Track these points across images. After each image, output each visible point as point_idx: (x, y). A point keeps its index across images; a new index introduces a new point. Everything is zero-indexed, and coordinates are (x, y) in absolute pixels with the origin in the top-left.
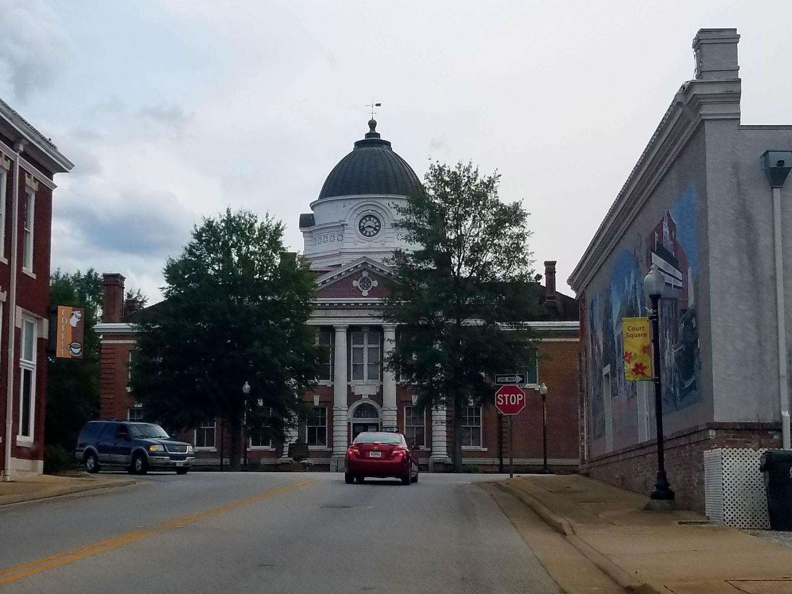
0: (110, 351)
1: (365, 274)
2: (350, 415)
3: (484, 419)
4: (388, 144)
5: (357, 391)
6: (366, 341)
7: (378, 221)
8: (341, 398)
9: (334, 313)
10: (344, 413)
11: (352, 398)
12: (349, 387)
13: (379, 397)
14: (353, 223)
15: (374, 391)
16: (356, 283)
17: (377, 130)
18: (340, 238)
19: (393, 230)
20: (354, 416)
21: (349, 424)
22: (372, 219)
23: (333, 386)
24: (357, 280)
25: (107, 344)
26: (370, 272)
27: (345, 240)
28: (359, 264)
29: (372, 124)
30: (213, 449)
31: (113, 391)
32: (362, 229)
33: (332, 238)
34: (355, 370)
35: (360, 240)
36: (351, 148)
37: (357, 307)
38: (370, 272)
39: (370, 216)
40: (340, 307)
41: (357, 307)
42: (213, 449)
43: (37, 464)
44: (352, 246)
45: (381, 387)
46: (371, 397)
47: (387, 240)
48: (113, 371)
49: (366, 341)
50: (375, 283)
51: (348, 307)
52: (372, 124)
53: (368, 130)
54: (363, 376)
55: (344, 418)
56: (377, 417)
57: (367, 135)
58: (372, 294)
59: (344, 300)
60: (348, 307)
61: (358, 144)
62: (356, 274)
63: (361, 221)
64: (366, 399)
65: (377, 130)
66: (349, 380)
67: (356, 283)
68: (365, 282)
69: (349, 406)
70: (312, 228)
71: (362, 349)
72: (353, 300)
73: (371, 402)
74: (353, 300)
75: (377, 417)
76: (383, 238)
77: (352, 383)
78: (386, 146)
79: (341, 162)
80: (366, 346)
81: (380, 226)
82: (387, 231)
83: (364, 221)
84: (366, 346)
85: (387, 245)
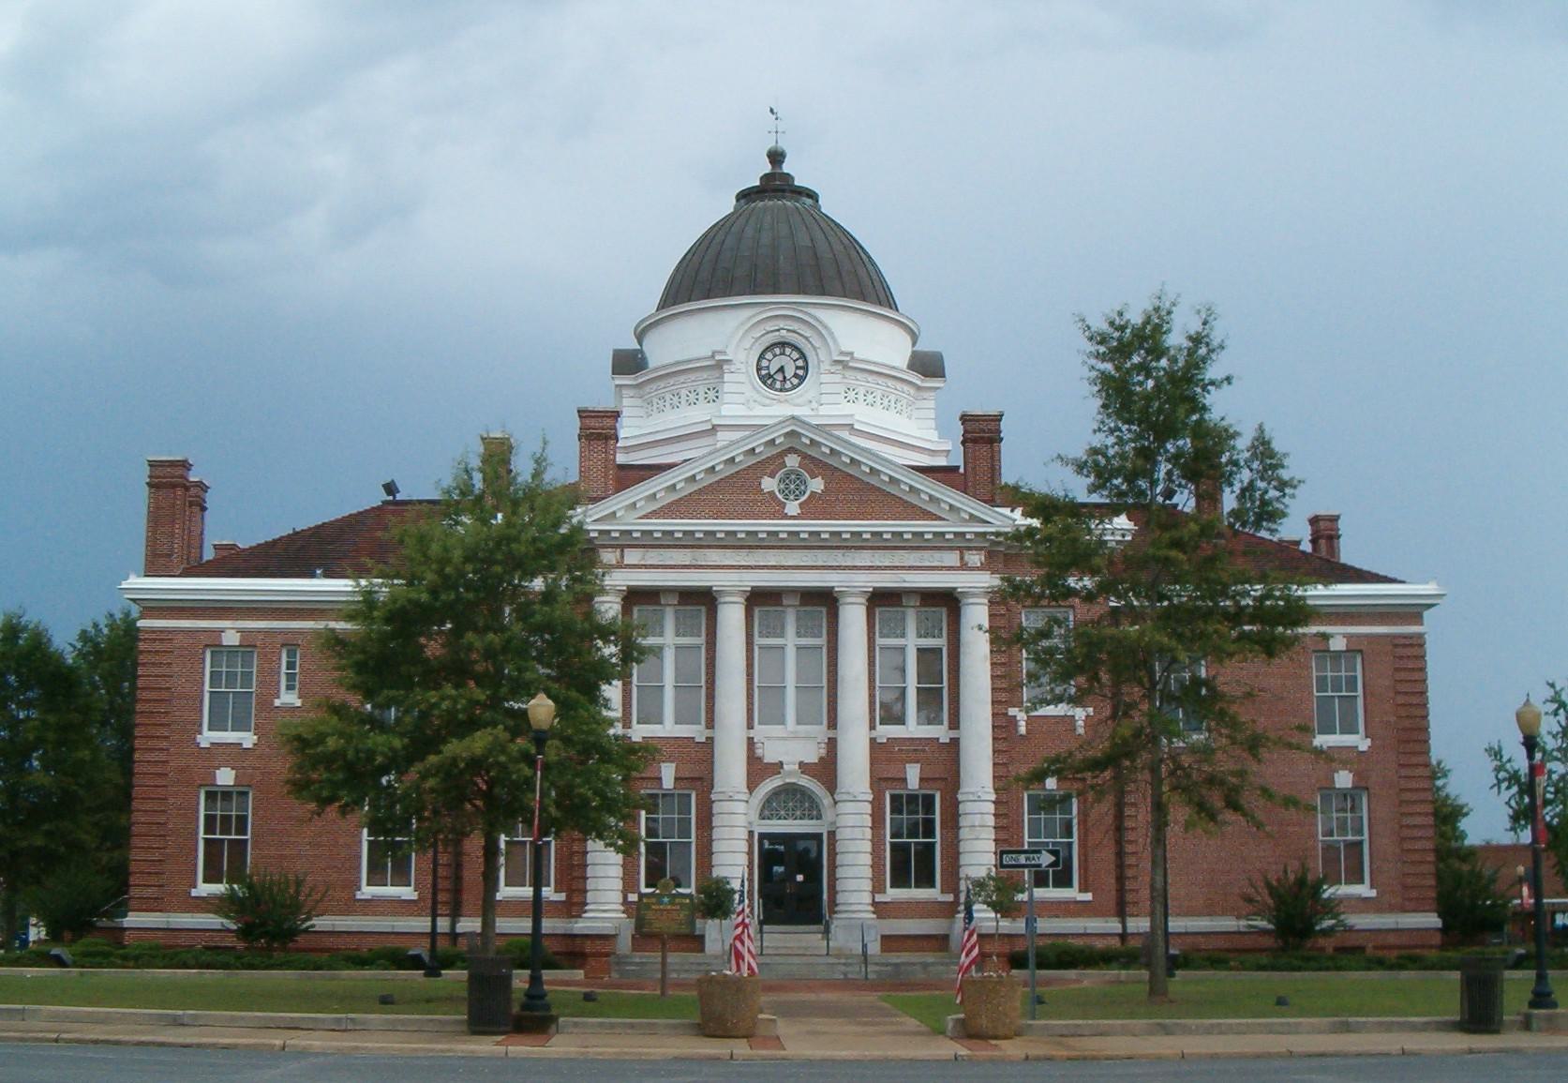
0: (157, 646)
1: (792, 461)
2: (754, 816)
3: (1083, 822)
4: (812, 195)
5: (770, 754)
6: (791, 629)
7: (803, 356)
8: (731, 770)
9: (714, 556)
10: (741, 807)
11: (758, 769)
12: (751, 742)
13: (827, 769)
14: (743, 358)
15: (812, 754)
16: (769, 484)
17: (786, 168)
18: (711, 395)
19: (837, 378)
20: (762, 817)
21: (751, 833)
22: (788, 351)
23: (710, 740)
24: (772, 476)
25: (153, 631)
26: (804, 456)
27: (727, 398)
28: (777, 435)
29: (776, 157)
30: (407, 893)
31: (164, 744)
32: (767, 379)
33: (692, 396)
34: (763, 703)
35: (756, 396)
36: (727, 205)
37: (773, 542)
38: (804, 456)
39: (783, 344)
40: (731, 542)
41: (773, 542)
42: (407, 893)
43: (1562, 968)
44: (741, 411)
45: (832, 744)
46: (805, 768)
47: (824, 399)
48: (165, 695)
49: (791, 629)
50: (817, 485)
51: (753, 543)
52: (776, 157)
53: (768, 168)
54: (784, 715)
55: (741, 820)
56: (819, 817)
57: (765, 178)
58: (809, 510)
59: (741, 525)
60: (753, 543)
61: (745, 196)
62: (771, 464)
63: (761, 357)
64: (790, 773)
65: (786, 168)
66: (750, 727)
67: (769, 484)
68: (793, 483)
69: (752, 785)
70: (642, 377)
71: (782, 648)
72: (764, 525)
73: (805, 781)
74: (764, 525)
75: (819, 817)
76: (809, 396)
77: (760, 731)
78: (809, 201)
79: (705, 235)
80: (791, 640)
81: (806, 368)
82: (825, 378)
83: (769, 356)
84: (791, 640)
85: (823, 410)
